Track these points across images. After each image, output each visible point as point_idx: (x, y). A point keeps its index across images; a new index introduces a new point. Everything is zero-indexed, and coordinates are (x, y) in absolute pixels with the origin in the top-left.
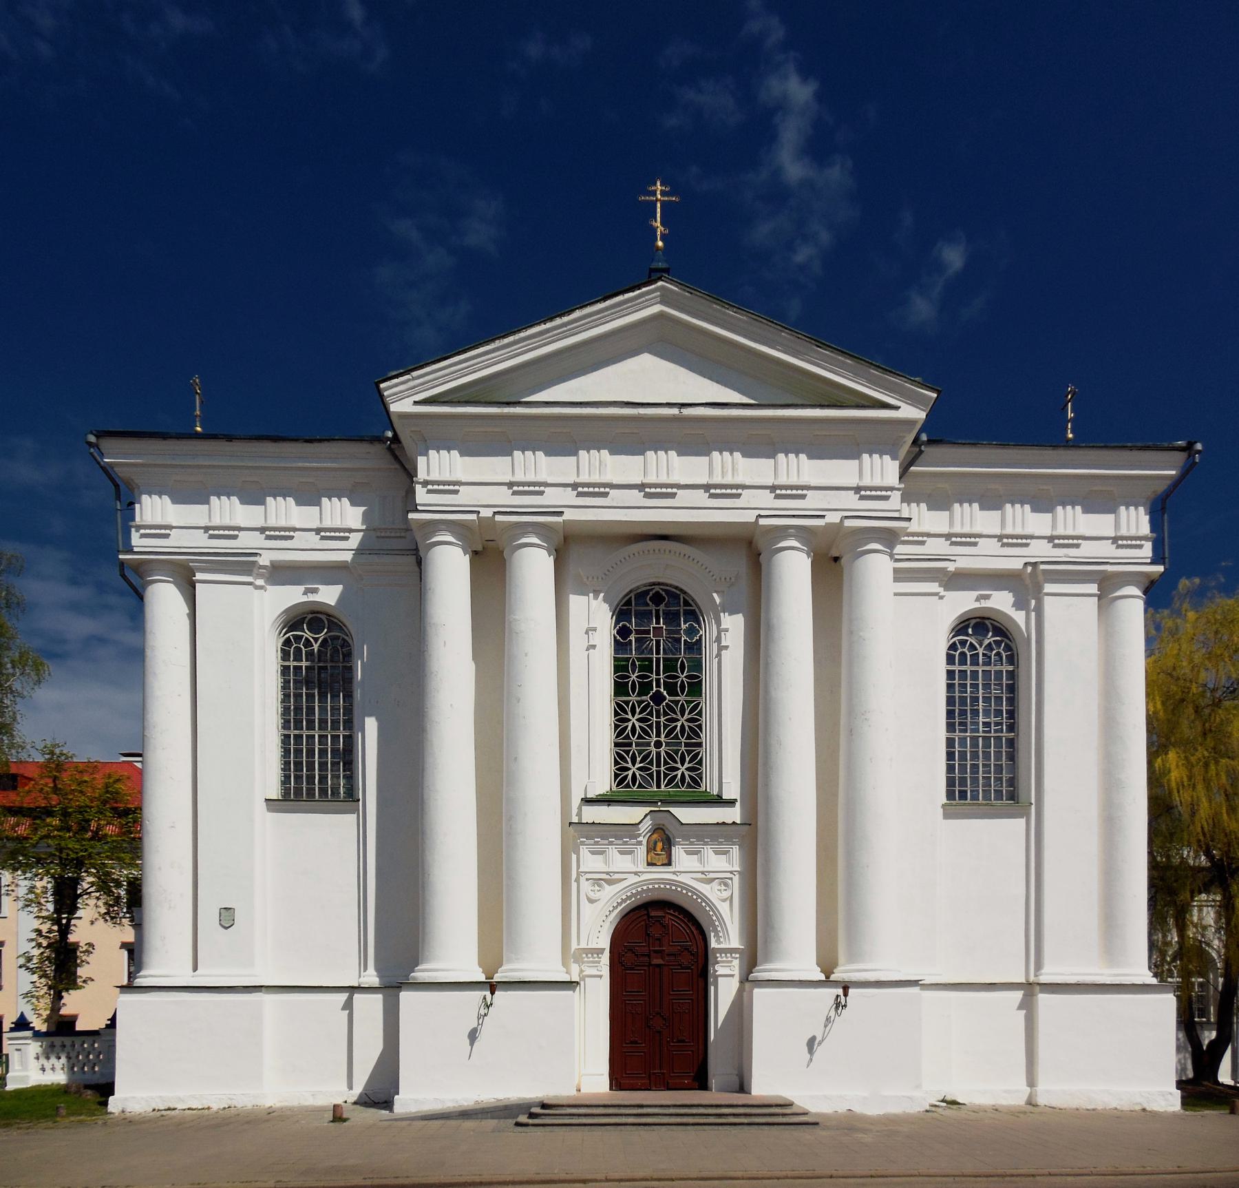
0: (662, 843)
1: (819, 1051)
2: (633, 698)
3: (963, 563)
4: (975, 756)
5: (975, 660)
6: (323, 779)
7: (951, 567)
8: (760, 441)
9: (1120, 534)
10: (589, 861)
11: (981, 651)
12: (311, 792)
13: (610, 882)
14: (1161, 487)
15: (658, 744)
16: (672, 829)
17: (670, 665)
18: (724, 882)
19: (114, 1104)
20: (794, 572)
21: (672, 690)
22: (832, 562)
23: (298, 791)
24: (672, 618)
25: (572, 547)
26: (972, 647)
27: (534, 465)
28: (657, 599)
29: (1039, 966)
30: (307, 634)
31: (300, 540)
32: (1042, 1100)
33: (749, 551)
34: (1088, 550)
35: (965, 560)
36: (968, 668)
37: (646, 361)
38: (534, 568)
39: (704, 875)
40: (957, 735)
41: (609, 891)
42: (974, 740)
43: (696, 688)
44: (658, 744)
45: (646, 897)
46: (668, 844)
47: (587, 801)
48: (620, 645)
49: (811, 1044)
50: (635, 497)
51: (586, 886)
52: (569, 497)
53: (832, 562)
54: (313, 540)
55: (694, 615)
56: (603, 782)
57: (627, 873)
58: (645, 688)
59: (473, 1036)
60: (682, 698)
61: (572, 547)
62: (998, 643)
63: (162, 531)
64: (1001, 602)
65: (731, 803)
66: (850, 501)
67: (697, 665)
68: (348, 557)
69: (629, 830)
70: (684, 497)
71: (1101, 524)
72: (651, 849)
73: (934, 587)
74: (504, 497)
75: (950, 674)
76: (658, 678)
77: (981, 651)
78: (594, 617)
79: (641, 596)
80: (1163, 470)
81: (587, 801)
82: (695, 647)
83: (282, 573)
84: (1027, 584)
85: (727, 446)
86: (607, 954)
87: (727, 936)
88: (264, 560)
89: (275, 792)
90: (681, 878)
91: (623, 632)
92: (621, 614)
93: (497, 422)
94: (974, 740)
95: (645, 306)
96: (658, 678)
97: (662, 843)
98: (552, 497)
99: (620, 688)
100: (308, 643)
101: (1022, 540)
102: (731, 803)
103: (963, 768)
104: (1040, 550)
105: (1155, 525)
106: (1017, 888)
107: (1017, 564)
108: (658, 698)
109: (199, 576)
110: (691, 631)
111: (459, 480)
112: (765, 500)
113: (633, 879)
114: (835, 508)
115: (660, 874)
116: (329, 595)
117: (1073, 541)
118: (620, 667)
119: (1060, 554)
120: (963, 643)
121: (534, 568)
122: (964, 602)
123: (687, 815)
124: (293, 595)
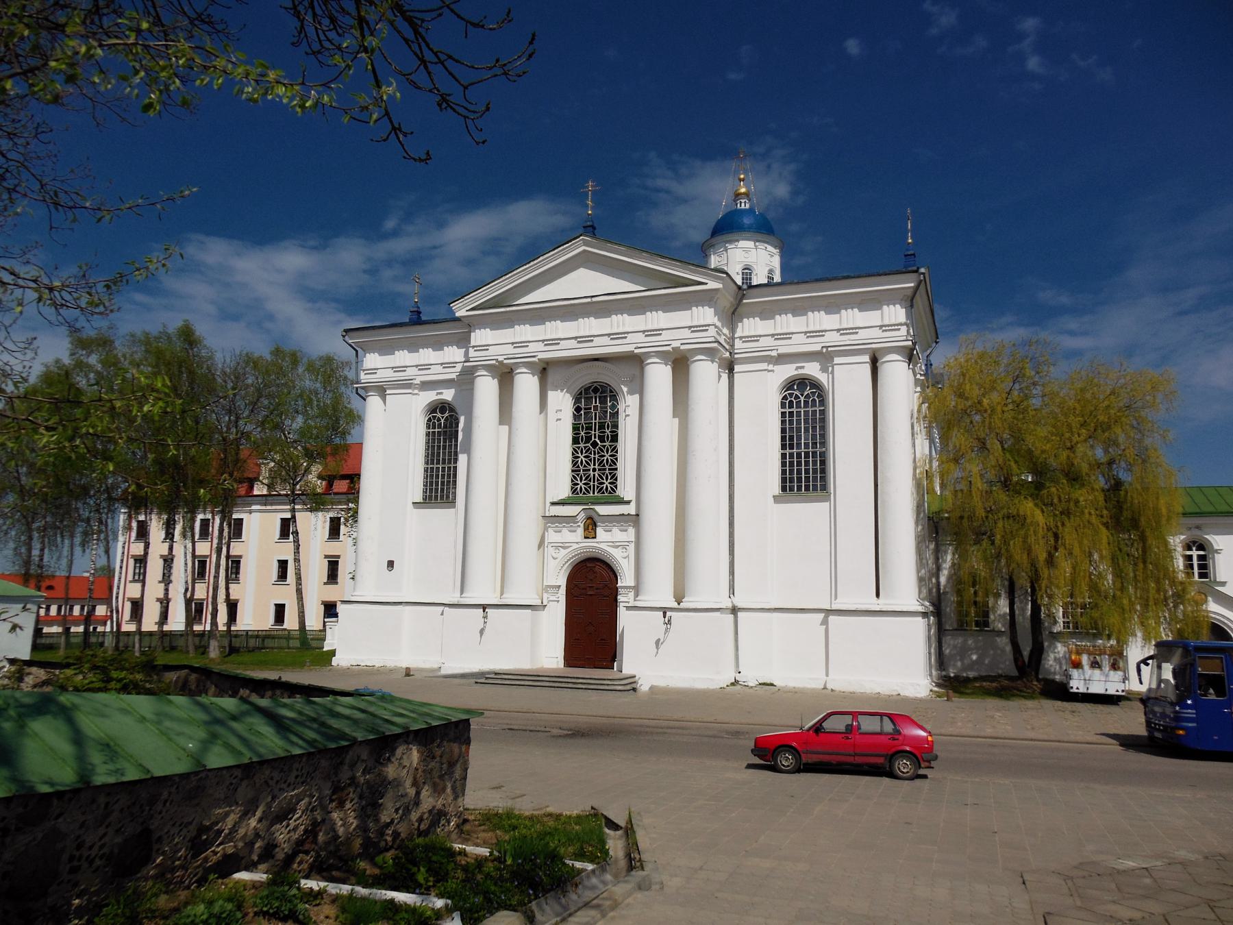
0: (591, 526)
1: (662, 648)
2: (582, 445)
3: (782, 350)
4: (799, 464)
5: (798, 406)
6: (442, 490)
7: (774, 353)
8: (635, 306)
9: (887, 322)
10: (552, 536)
11: (802, 399)
12: (436, 497)
13: (564, 548)
14: (910, 293)
15: (594, 470)
16: (596, 518)
17: (602, 426)
18: (624, 547)
19: (335, 661)
20: (659, 376)
21: (602, 439)
22: (680, 363)
23: (430, 497)
24: (603, 401)
25: (545, 370)
26: (797, 397)
27: (524, 332)
28: (596, 390)
29: (628, 608)
30: (439, 415)
31: (434, 369)
32: (829, 686)
33: (635, 362)
34: (863, 335)
35: (785, 348)
36: (794, 410)
37: (582, 272)
38: (526, 384)
39: (611, 542)
40: (788, 451)
41: (563, 552)
42: (799, 455)
43: (615, 438)
44: (594, 470)
45: (584, 556)
46: (595, 525)
47: (553, 504)
48: (576, 417)
49: (658, 643)
50: (573, 343)
51: (551, 549)
52: (541, 347)
53: (680, 363)
54: (439, 369)
55: (614, 398)
56: (565, 492)
57: (573, 542)
58: (588, 439)
59: (482, 632)
60: (607, 444)
61: (545, 370)
62: (813, 393)
63: (374, 371)
64: (812, 369)
65: (628, 502)
66: (686, 334)
67: (616, 426)
68: (454, 376)
69: (572, 519)
70: (597, 341)
71: (872, 317)
72: (586, 529)
73: (764, 366)
74: (509, 350)
75: (783, 414)
76: (595, 434)
77: (802, 399)
78: (562, 403)
79: (587, 390)
80: (907, 284)
81: (553, 504)
82: (615, 415)
83: (426, 386)
84: (825, 357)
85: (620, 311)
86: (563, 590)
87: (626, 579)
88: (417, 381)
89: (419, 498)
90: (602, 546)
91: (578, 409)
92: (577, 400)
93: (503, 313)
94: (799, 455)
95: (578, 247)
96: (595, 434)
97: (591, 526)
98: (532, 347)
99: (575, 440)
100: (439, 420)
101: (820, 333)
102: (628, 502)
103: (791, 472)
104: (832, 339)
105: (908, 316)
106: (826, 547)
107: (817, 348)
108: (595, 444)
109: (388, 392)
110: (613, 407)
111: (492, 342)
112: (640, 338)
113: (575, 546)
114: (676, 339)
115: (590, 543)
116: (448, 395)
117: (854, 330)
118: (576, 428)
119: (847, 339)
120: (791, 395)
121: (526, 384)
122: (788, 371)
123: (603, 510)
124: (431, 396)
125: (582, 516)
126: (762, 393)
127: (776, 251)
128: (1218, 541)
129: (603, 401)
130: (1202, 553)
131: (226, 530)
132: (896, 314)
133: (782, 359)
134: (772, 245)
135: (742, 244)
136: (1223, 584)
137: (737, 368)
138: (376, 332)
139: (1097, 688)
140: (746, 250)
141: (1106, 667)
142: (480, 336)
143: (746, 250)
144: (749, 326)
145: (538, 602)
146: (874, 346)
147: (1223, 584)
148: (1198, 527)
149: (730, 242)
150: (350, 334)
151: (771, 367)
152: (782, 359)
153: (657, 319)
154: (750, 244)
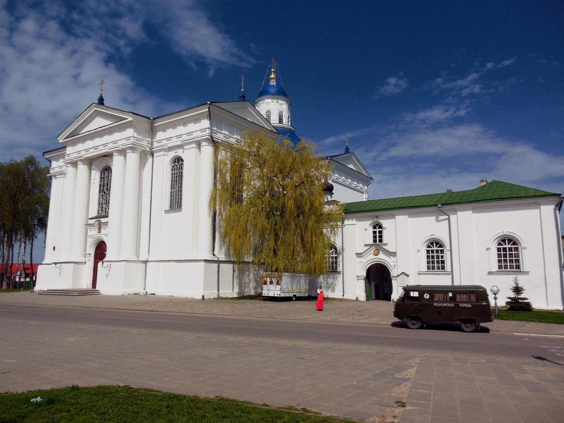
3: (169, 145)
7: (166, 147)
24: (108, 173)
39: (93, 232)
73: (163, 153)
114: (121, 144)
115: (99, 235)
125: (96, 223)
126: (162, 164)
127: (284, 103)
128: (384, 222)
129: (108, 173)
130: (380, 230)
131: (231, 251)
132: (205, 123)
133: (170, 149)
134: (280, 99)
135: (266, 101)
136: (386, 244)
137: (155, 155)
138: (61, 150)
139: (271, 294)
140: (268, 104)
141: (275, 284)
142: (69, 150)
143: (268, 104)
144: (160, 135)
145: (83, 261)
146: (196, 139)
147: (386, 244)
148: (377, 217)
149: (261, 100)
150: (45, 154)
151: (166, 153)
152: (170, 149)
153: (117, 136)
154: (270, 100)
